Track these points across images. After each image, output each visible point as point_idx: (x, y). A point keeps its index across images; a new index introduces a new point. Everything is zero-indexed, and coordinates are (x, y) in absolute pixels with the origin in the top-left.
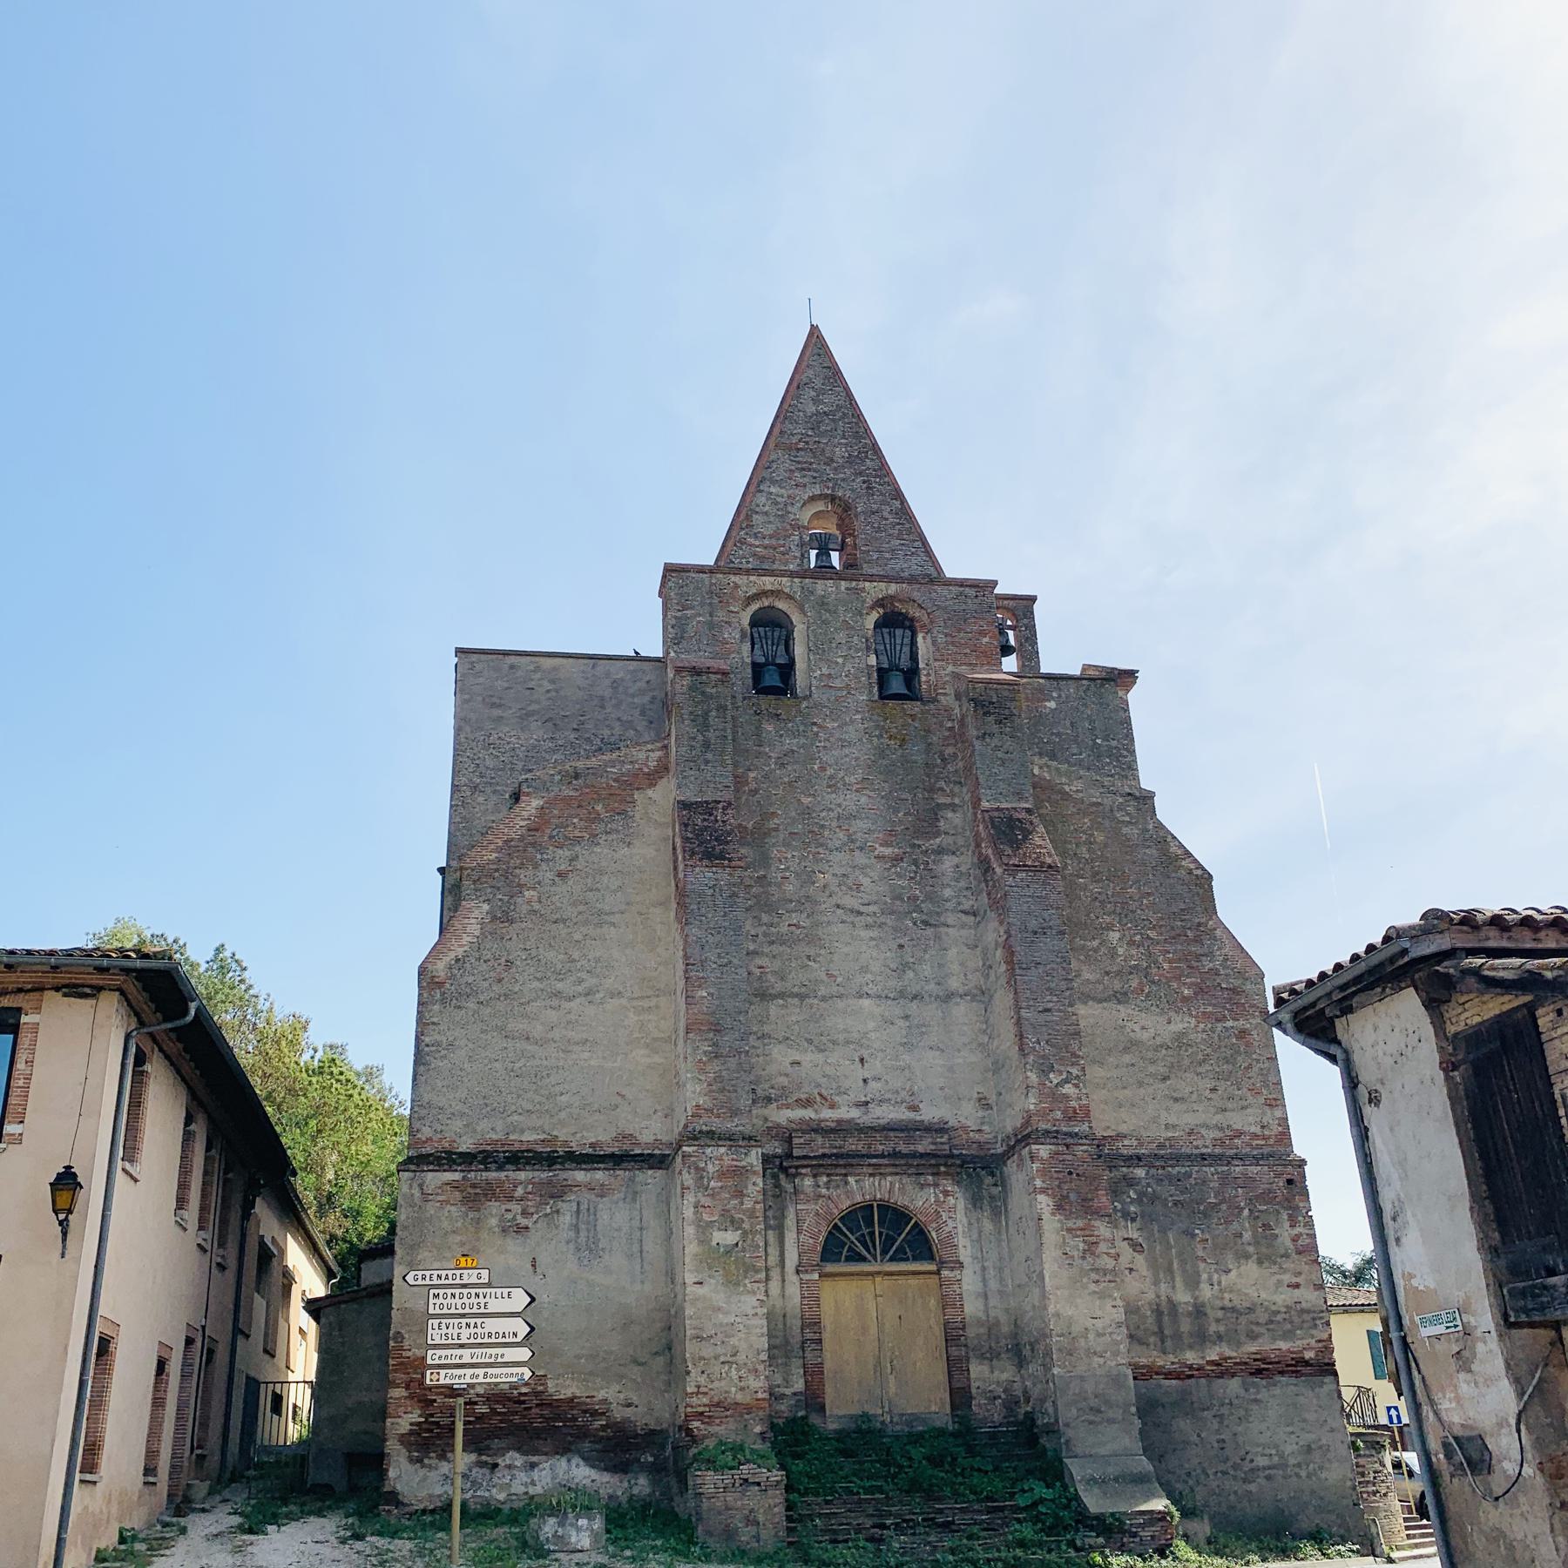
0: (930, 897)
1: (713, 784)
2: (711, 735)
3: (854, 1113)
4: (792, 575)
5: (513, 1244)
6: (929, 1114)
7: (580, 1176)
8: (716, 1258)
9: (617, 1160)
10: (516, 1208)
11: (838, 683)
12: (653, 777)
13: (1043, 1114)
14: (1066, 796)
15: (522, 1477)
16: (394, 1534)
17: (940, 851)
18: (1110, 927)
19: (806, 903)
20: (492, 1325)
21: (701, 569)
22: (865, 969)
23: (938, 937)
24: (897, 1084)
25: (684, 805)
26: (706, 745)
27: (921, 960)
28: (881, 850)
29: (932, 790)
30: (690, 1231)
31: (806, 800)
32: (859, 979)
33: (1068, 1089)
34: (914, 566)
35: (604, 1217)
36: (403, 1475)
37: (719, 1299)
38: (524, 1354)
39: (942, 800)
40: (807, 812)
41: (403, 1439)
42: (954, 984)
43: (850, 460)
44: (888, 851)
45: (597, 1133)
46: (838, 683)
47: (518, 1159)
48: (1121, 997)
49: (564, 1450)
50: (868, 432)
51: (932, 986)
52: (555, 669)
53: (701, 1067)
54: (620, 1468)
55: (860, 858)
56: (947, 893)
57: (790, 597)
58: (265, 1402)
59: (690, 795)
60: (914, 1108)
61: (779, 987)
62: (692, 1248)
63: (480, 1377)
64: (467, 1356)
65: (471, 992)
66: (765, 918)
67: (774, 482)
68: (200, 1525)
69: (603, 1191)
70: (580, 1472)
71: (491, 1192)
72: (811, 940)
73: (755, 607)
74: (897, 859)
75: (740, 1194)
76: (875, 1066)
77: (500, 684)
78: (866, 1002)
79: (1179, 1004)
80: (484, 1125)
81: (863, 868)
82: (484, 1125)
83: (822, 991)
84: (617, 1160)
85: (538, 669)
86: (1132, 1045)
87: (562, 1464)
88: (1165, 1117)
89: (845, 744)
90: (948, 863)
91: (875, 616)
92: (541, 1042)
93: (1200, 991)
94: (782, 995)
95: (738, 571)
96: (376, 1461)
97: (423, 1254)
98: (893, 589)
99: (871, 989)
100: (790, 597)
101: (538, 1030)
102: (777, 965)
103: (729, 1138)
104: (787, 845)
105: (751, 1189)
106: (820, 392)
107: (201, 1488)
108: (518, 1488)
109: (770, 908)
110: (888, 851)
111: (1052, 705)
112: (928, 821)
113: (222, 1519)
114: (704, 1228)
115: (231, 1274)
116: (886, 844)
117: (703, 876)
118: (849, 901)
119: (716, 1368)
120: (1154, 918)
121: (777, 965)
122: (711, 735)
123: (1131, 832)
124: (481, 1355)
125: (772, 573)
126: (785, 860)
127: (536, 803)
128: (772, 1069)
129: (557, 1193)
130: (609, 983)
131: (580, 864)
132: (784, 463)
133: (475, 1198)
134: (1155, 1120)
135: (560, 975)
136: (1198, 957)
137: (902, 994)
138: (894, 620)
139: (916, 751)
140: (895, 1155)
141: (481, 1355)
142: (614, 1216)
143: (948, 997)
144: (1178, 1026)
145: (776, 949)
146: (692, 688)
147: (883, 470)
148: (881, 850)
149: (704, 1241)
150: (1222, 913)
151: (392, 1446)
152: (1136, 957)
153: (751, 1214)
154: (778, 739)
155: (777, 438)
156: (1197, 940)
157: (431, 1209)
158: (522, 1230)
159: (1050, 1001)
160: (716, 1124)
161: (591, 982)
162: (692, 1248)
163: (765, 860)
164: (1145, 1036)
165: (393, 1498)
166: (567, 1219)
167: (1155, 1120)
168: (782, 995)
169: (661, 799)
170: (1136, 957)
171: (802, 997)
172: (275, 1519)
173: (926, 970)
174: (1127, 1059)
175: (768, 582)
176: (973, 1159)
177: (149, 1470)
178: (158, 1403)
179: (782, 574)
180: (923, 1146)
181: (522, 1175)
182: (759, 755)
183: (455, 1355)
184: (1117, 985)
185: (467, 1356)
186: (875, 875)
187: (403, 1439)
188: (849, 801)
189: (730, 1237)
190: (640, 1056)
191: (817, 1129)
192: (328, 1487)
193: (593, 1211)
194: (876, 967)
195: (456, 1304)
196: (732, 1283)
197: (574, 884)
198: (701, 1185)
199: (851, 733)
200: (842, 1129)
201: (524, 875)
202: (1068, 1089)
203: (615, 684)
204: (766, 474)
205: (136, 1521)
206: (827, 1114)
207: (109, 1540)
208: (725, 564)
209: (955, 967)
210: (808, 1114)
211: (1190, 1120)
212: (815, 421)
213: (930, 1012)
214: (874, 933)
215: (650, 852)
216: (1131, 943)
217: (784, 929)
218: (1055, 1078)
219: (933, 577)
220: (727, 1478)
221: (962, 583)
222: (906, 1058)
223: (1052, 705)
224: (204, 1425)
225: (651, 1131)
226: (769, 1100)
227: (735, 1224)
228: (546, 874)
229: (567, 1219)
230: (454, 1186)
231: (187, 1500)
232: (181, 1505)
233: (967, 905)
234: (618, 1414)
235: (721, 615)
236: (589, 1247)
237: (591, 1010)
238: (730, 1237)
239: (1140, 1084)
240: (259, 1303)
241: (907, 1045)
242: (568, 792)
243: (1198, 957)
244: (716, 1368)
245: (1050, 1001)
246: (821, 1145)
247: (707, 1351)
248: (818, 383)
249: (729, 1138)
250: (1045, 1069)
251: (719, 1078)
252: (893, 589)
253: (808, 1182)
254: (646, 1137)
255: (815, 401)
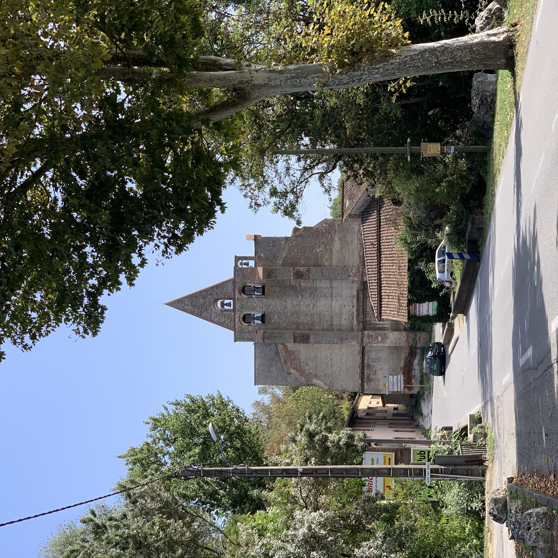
0: (310, 289)
1: (289, 334)
2: (278, 336)
3: (355, 308)
4: (235, 314)
5: (378, 373)
6: (355, 293)
7: (366, 361)
8: (383, 341)
9: (363, 355)
10: (371, 373)
11: (261, 305)
12: (285, 346)
13: (358, 277)
14: (286, 257)
15: (416, 371)
16: (424, 393)
17: (300, 286)
18: (316, 251)
19: (312, 315)
20: (395, 381)
21: (235, 334)
22: (326, 304)
23: (319, 288)
24: (349, 299)
25: (295, 342)
26: (280, 337)
27: (324, 292)
28: (300, 299)
29: (286, 286)
30: (378, 345)
31: (289, 314)
32: (328, 305)
33: (353, 271)
34: (230, 285)
35: (373, 357)
36: (415, 391)
37: (390, 340)
38: (399, 376)
39: (288, 284)
40: (292, 314)
41: (409, 391)
42: (329, 286)
43: (204, 298)
44: (300, 297)
45: (358, 358)
46: (261, 305)
47: (362, 373)
48: (331, 250)
49: (412, 364)
50: (196, 293)
51: (330, 290)
52: (258, 365)
53: (349, 342)
54: (416, 354)
55: (302, 303)
56: (309, 285)
57: (240, 315)
58: (396, 412)
59: (292, 340)
60: (354, 296)
61: (330, 322)
62: (381, 345)
63: (402, 383)
64: (399, 385)
65: (331, 382)
66: (315, 324)
67: (211, 317)
68: (421, 423)
69: (369, 357)
70: (416, 361)
71: (368, 377)
72: (320, 314)
73: (242, 322)
74: (302, 295)
75: (372, 336)
76: (345, 303)
77: (262, 376)
78: (333, 304)
79: (332, 239)
80: (356, 379)
81: (304, 303)
82: (356, 379)
83: (331, 313)
84: (363, 355)
85: (258, 369)
86: (341, 249)
87: (414, 365)
88: (356, 245)
89: (276, 305)
90: (302, 284)
91: (243, 295)
92: (341, 368)
93: (329, 233)
94: (331, 321)
95: (235, 326)
96: (412, 396)
97: (379, 389)
98: (237, 291)
99: (330, 303)
100: (240, 315)
101: (339, 369)
102: (325, 322)
103: (362, 337)
104: (299, 319)
105: (372, 334)
106: (185, 304)
107: (415, 424)
108: (418, 372)
109: (313, 323)
110: (300, 297)
111: (262, 255)
112: (293, 288)
113: (421, 419)
114: (378, 342)
115: (376, 421)
116: (299, 298)
117: (312, 340)
118: (312, 306)
119: (401, 341)
120: (314, 241)
121: (325, 322)
122: (278, 336)
123: (294, 243)
124: (399, 383)
125: (235, 319)
126: (303, 319)
127: (292, 370)
128: (346, 324)
129: (369, 365)
130: (329, 355)
131: (305, 361)
132: (205, 314)
133: (369, 380)
134: (356, 247)
135: (328, 365)
136: (322, 233)
137: (331, 297)
138: (243, 290)
139: (277, 289)
140: (363, 301)
141: (399, 383)
142: (373, 355)
143: (331, 287)
144: (337, 239)
145: (322, 322)
146: (267, 339)
147: (206, 291)
148: (300, 299)
149: (380, 342)
150: (313, 225)
151: (411, 393)
152: (322, 246)
153: (376, 334)
154: (275, 319)
155: (200, 315)
156: (319, 232)
157: (371, 388)
158: (375, 371)
159: (336, 273)
160: (360, 340)
161: (329, 359)
162: (381, 345)
163: (303, 324)
164: (339, 246)
165: (419, 392)
166: (374, 364)
167: (356, 247)
168: (331, 321)
169: (291, 345)
170: (322, 246)
171: (332, 317)
172: (421, 411)
173: (326, 291)
174: (344, 251)
175: (237, 320)
176: (364, 286)
177: (413, 432)
178: (402, 431)
179: (235, 317)
180: (361, 295)
181: (366, 372)
182: (279, 324)
183: (399, 387)
184: (328, 251)
185: (399, 385)
186: (306, 301)
187: (409, 391)
188: (289, 304)
189: (380, 338)
190: (343, 350)
191: (358, 315)
192: (416, 401)
193: (372, 359)
194: (326, 302)
195: (391, 387)
196: (387, 338)
197: (309, 362)
198: (371, 343)
199: (273, 303)
200: (358, 311)
201: (307, 372)
202: (353, 271)
203: (261, 352)
204: (209, 318)
205: (420, 433)
206: (355, 314)
207: (423, 436)
208: (233, 329)
209: (325, 285)
210: (355, 317)
211: (356, 240)
212: (194, 306)
213: (335, 291)
214: (318, 301)
215: (302, 347)
216: (319, 247)
217: (317, 320)
218: (351, 274)
219: (233, 281)
220: (418, 342)
221: (235, 275)
222: (344, 297)
223: (262, 255)
224: (404, 424)
225: (358, 348)
226: (352, 325)
227: (377, 337)
228: (307, 368)
229: (374, 364)
230: (367, 384)
231: (417, 425)
232: (418, 426)
233: (312, 281)
234: (407, 355)
235: (246, 330)
236: (378, 360)
237: (335, 359)
238: (380, 338)
239: (349, 249)
240: (377, 414)
241: (342, 296)
242: (289, 364)
243: (322, 233)
244: (401, 341)
245: (336, 273)
246: (361, 316)
247: (398, 342)
248: (183, 305)
249: (362, 337)
250: (350, 276)
251: (351, 339)
252: (237, 291)
253: (368, 319)
254: (359, 349)
255: (188, 305)
